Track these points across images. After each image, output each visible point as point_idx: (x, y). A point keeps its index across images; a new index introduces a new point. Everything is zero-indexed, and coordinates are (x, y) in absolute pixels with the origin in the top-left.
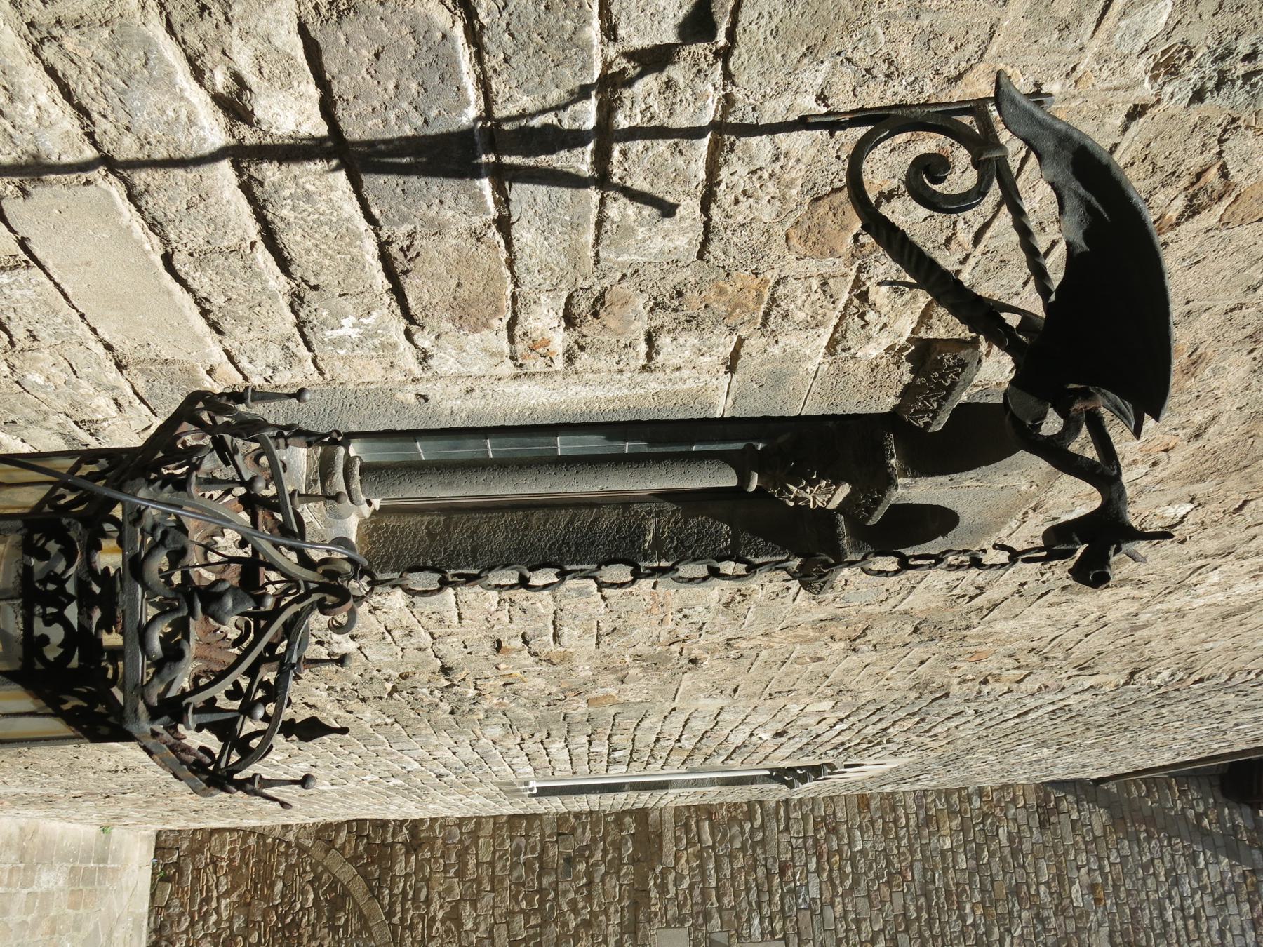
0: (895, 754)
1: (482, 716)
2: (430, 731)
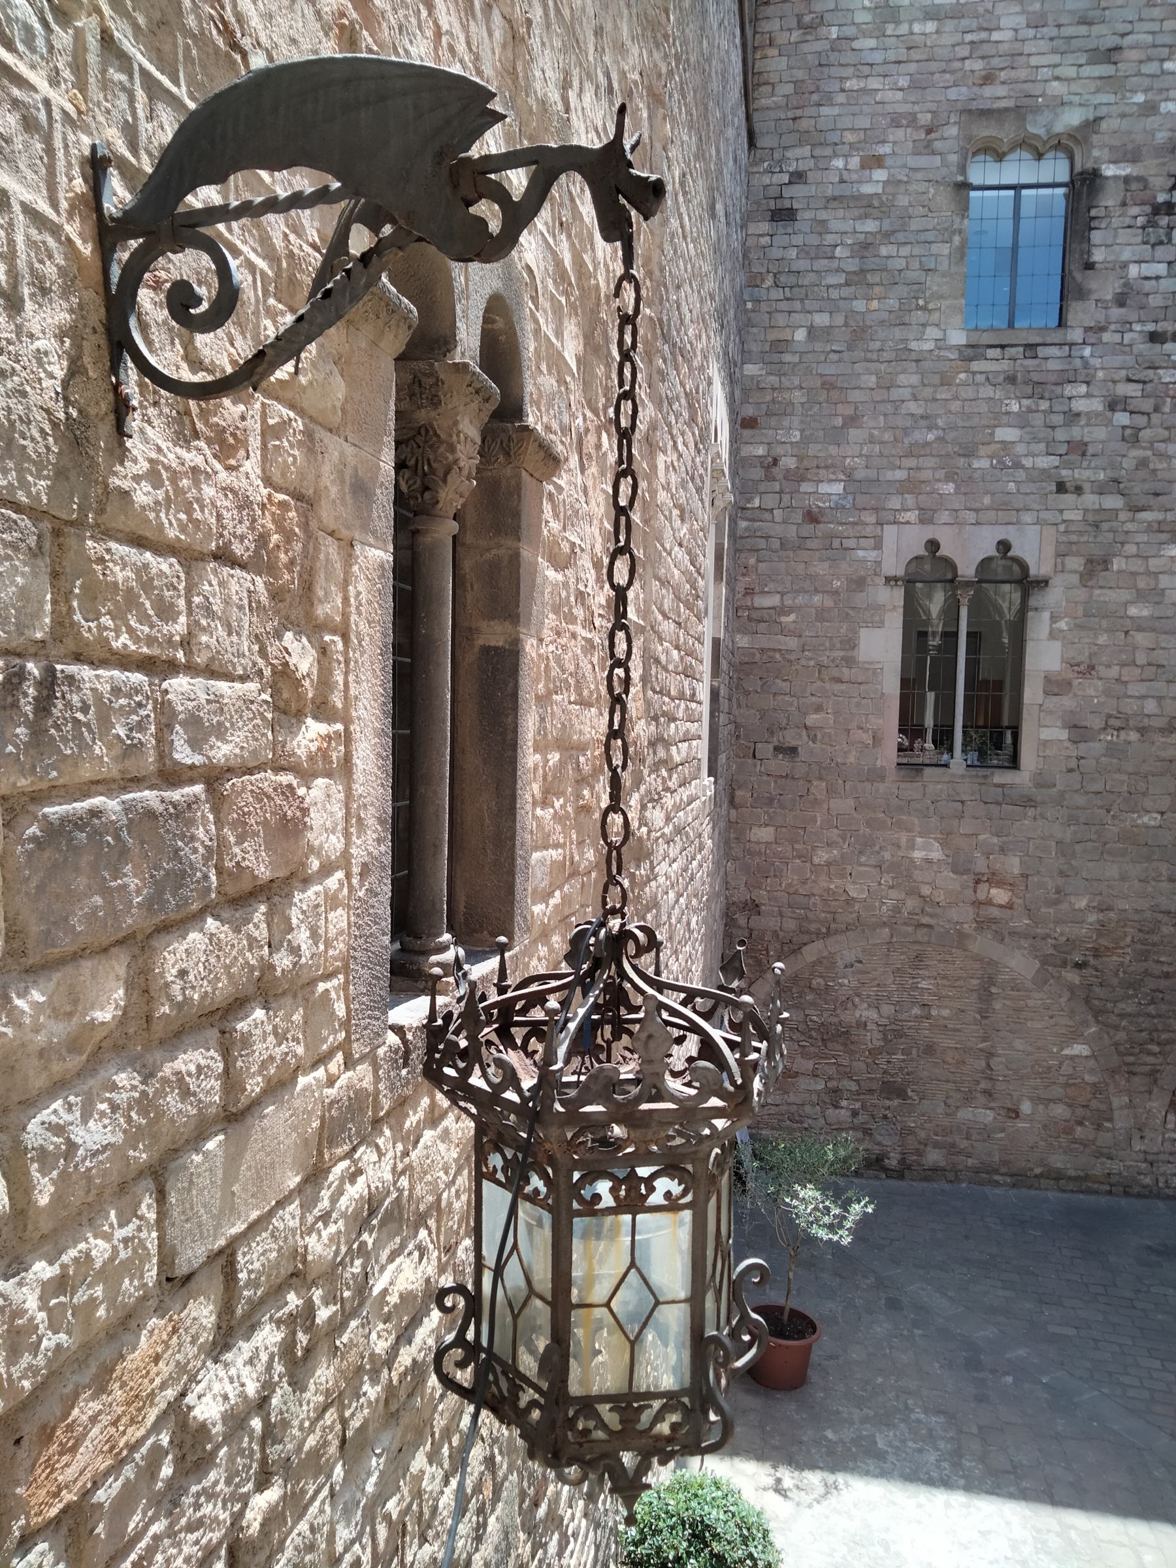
0: (710, 383)
1: (644, 829)
2: (653, 884)
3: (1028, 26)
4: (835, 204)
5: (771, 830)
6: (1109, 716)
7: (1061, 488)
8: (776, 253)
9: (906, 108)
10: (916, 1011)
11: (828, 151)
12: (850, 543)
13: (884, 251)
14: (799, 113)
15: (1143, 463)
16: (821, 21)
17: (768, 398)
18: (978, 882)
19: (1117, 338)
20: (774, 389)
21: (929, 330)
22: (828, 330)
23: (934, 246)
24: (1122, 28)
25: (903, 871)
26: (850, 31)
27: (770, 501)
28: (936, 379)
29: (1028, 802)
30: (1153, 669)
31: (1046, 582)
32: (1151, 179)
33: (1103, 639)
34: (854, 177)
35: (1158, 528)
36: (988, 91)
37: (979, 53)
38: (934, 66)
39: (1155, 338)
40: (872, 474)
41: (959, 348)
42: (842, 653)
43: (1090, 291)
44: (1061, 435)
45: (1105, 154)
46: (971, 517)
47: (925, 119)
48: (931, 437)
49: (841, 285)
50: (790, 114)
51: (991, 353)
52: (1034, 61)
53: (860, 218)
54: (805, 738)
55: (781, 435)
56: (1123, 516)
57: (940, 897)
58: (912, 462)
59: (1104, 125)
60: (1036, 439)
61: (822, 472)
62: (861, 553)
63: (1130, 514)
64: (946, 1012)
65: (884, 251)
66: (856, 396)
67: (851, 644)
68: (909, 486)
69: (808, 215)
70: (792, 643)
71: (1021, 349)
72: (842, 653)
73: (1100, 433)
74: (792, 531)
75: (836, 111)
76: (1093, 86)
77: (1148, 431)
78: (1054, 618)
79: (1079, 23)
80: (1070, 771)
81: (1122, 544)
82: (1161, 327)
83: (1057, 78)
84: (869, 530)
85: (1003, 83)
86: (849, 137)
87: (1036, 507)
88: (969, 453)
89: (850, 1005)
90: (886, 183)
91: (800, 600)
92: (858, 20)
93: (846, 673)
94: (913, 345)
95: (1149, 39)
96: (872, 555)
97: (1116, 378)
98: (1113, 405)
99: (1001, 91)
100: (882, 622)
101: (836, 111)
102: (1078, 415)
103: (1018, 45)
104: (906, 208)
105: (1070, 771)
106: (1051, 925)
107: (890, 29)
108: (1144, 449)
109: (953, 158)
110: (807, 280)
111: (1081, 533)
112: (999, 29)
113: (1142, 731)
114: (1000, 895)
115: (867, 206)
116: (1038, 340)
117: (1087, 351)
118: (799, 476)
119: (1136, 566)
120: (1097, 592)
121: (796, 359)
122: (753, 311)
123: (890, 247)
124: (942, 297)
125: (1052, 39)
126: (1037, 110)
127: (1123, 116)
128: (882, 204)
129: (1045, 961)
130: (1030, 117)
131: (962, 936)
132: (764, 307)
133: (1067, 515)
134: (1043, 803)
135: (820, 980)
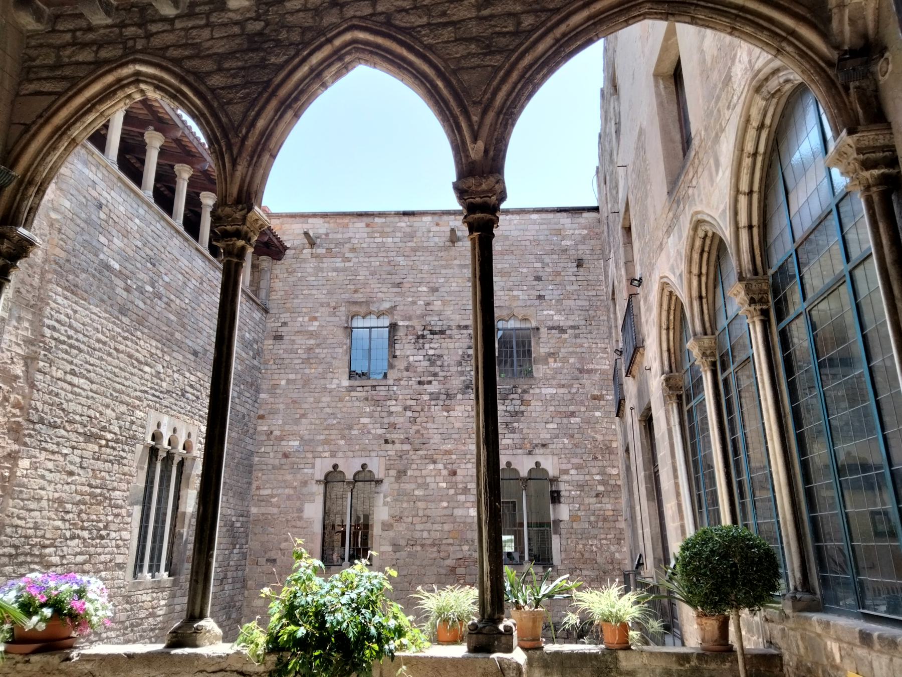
6: (409, 539)
7: (386, 442)
8: (275, 352)
11: (296, 315)
13: (317, 351)
15: (418, 431)
19: (406, 383)
24: (403, 276)
26: (305, 274)
27: (269, 449)
28: (337, 399)
31: (382, 481)
33: (405, 505)
35: (425, 457)
36: (356, 296)
40: (311, 437)
41: (346, 387)
44: (386, 420)
46: (351, 454)
48: (335, 422)
51: (358, 389)
52: (372, 286)
56: (411, 453)
58: (327, 432)
61: (291, 437)
62: (306, 470)
65: (317, 351)
66: (305, 406)
67: (300, 510)
68: (327, 442)
69: (288, 338)
70: (275, 510)
73: (401, 420)
74: (277, 462)
76: (393, 295)
78: (385, 497)
82: (422, 379)
84: (309, 461)
86: (304, 310)
88: (350, 428)
91: (280, 491)
93: (298, 524)
94: (328, 386)
96: (310, 471)
99: (360, 295)
107: (320, 274)
109: (344, 318)
110: (288, 361)
113: (422, 546)
115: (311, 335)
117: (395, 388)
118: (281, 439)
119: (417, 473)
126: (373, 302)
133: (390, 453)
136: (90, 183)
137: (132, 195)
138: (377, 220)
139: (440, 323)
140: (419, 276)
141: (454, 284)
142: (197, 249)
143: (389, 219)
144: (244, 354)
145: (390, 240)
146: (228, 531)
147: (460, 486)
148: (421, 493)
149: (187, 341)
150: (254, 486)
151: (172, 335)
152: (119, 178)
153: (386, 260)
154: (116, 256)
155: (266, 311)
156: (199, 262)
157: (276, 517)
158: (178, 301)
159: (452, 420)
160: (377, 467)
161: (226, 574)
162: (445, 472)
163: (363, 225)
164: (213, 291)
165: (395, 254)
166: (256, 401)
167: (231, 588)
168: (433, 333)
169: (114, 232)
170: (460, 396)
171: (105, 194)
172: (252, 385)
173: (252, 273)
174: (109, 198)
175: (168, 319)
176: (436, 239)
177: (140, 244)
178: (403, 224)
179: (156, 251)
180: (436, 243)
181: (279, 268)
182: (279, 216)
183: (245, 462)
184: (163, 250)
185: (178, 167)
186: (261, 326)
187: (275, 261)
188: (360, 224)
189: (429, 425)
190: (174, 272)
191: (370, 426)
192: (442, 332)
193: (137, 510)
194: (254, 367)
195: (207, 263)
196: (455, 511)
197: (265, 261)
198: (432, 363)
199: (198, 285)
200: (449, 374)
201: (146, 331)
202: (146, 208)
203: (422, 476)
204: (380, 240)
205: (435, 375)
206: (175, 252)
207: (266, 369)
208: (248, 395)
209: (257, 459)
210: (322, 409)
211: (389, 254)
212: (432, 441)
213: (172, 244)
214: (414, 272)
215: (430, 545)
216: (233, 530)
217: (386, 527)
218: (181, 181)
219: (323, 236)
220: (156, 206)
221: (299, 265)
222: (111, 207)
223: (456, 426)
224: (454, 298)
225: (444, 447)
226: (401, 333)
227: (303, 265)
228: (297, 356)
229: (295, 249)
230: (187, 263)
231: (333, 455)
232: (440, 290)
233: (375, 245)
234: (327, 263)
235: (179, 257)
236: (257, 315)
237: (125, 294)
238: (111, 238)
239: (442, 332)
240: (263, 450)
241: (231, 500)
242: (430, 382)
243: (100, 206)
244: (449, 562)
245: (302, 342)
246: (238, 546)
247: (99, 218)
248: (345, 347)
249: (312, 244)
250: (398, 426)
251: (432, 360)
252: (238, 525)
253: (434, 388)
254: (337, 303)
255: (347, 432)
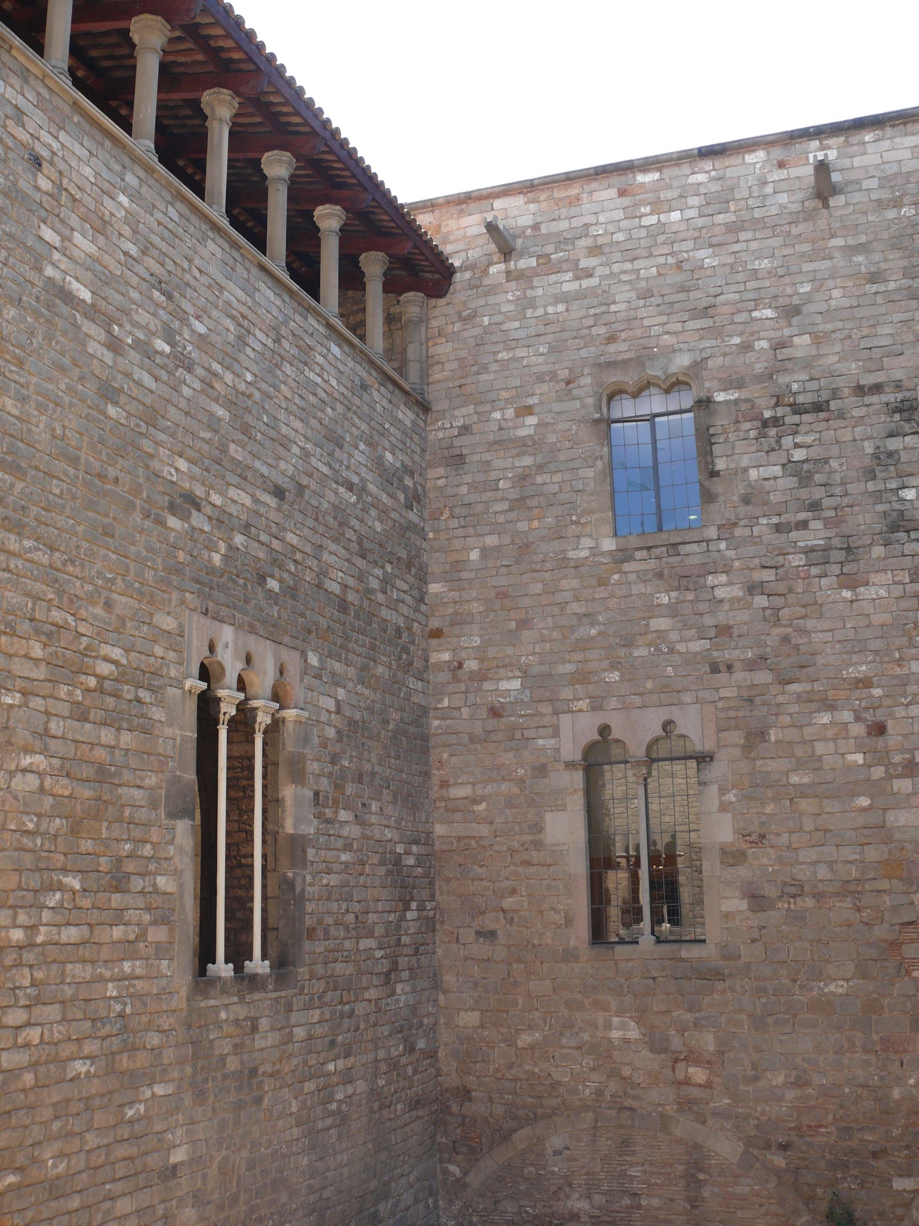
3: (638, 298)
4: (496, 447)
5: (477, 1014)
6: (785, 884)
7: (715, 669)
8: (450, 491)
9: (544, 369)
10: (626, 1201)
11: (487, 407)
12: (530, 733)
13: (539, 479)
14: (463, 381)
15: (785, 639)
16: (475, 315)
17: (451, 610)
18: (676, 1060)
19: (747, 532)
20: (455, 602)
21: (583, 540)
22: (498, 548)
23: (580, 471)
24: (712, 291)
25: (603, 1053)
26: (497, 319)
27: (458, 701)
28: (594, 582)
29: (718, 975)
30: (821, 834)
31: (712, 758)
32: (757, 401)
33: (769, 809)
34: (511, 424)
35: (804, 699)
36: (612, 348)
37: (602, 321)
38: (566, 335)
39: (778, 528)
40: (545, 669)
41: (610, 552)
42: (530, 837)
43: (717, 495)
44: (708, 621)
45: (715, 384)
46: (637, 700)
47: (564, 374)
48: (593, 632)
49: (506, 511)
50: (457, 383)
51: (638, 555)
52: (646, 322)
53: (518, 455)
54: (503, 921)
55: (464, 642)
56: (774, 689)
57: (639, 1077)
58: (579, 656)
59: (710, 363)
60: (686, 626)
61: (502, 672)
62: (541, 742)
63: (780, 687)
64: (655, 1202)
65: (539, 479)
66: (526, 602)
67: (538, 828)
68: (580, 678)
69: (476, 458)
70: (484, 830)
71: (664, 549)
72: (530, 837)
73: (743, 616)
74: (478, 728)
75: (492, 376)
76: (697, 336)
77: (786, 610)
78: (722, 791)
79: (678, 292)
80: (753, 941)
81: (776, 715)
82: (785, 518)
83: (667, 333)
84: (546, 721)
85: (624, 341)
86: (505, 394)
87: (693, 687)
88: (629, 643)
89: (562, 1196)
90: (537, 426)
91: (489, 789)
92: (504, 310)
93: (535, 856)
94: (571, 554)
95: (737, 297)
96: (551, 743)
97: (752, 566)
98: (753, 589)
99: (622, 347)
100: (565, 806)
101: (492, 376)
102: (721, 601)
103: (632, 313)
104: (554, 444)
105: (753, 941)
106: (751, 1104)
107: (529, 313)
108: (785, 626)
109: (590, 401)
110: (479, 508)
111: (738, 709)
112: (614, 303)
113: (819, 896)
114: (698, 1074)
115: (524, 445)
116: (679, 540)
117: (723, 545)
118: (481, 676)
119: (792, 734)
120: (759, 763)
121: (472, 575)
122: (434, 539)
123: (544, 476)
124: (591, 512)
125: (658, 305)
126: (652, 358)
127: (725, 355)
128: (535, 443)
129: (749, 1142)
130: (648, 364)
131: (665, 1119)
132: (443, 536)
133: (724, 693)
134: (731, 975)
135: (531, 1169)
136: (9, 110)
137: (108, 143)
138: (641, 178)
139: (814, 385)
140: (751, 285)
141: (836, 293)
142: (262, 268)
143: (668, 172)
144: (385, 498)
145: (676, 216)
146: (389, 873)
147: (897, 758)
148: (806, 780)
149: (257, 464)
150: (435, 780)
151: (224, 450)
152: (75, 105)
153: (671, 260)
154: (81, 272)
155: (423, 407)
156: (267, 294)
157: (485, 843)
158: (228, 377)
159: (868, 608)
160: (694, 726)
161: (395, 963)
162: (858, 730)
163: (613, 192)
164: (304, 357)
165: (690, 244)
166: (421, 600)
167: (408, 989)
168: (798, 410)
169: (74, 221)
170: (878, 551)
171: (45, 137)
172: (409, 565)
173: (389, 334)
174: (55, 145)
175: (212, 415)
176: (783, 198)
177: (133, 250)
178: (701, 178)
179: (170, 266)
180: (782, 207)
181: (442, 311)
182: (430, 205)
183: (412, 729)
184: (186, 265)
185: (207, 97)
186: (416, 438)
187: (433, 301)
188: (606, 194)
189: (810, 624)
190: (215, 313)
191: (674, 636)
192: (818, 407)
193: (185, 833)
194: (411, 527)
195: (287, 298)
196: (891, 817)
197: (412, 303)
198: (805, 480)
199: (270, 343)
200: (846, 500)
201: (161, 436)
202: (142, 173)
203: (804, 742)
204: (653, 219)
205: (814, 506)
206: (212, 270)
207: (437, 531)
208: (404, 586)
209: (436, 723)
210: (563, 605)
211: (676, 247)
212: (820, 660)
213: (205, 253)
214: (740, 277)
215: (836, 894)
216: (400, 872)
217: (732, 857)
218: (216, 124)
219: (529, 231)
220: (161, 169)
221: (482, 301)
222: (62, 166)
223: (877, 619)
224: (840, 325)
225: (852, 672)
226: (721, 420)
227: (492, 300)
228: (499, 494)
229: (471, 267)
230: (241, 295)
231: (596, 707)
232: (805, 309)
233: (643, 233)
234: (541, 288)
235: (222, 281)
236: (406, 415)
237: (108, 357)
238: (67, 232)
239: (818, 407)
240: (446, 703)
241: (389, 809)
242: (803, 525)
243: (37, 162)
244: (880, 932)
245: (506, 467)
246: (414, 905)
247: (37, 188)
248: (599, 464)
249: (507, 251)
250: (736, 632)
251: (802, 474)
252: (411, 861)
253: (816, 535)
254: (571, 370)
255: (622, 652)
